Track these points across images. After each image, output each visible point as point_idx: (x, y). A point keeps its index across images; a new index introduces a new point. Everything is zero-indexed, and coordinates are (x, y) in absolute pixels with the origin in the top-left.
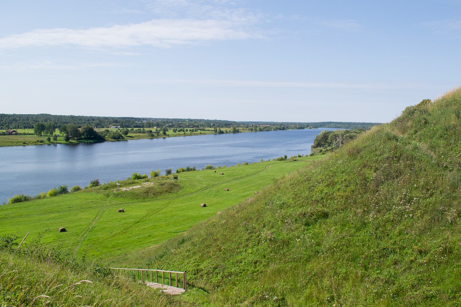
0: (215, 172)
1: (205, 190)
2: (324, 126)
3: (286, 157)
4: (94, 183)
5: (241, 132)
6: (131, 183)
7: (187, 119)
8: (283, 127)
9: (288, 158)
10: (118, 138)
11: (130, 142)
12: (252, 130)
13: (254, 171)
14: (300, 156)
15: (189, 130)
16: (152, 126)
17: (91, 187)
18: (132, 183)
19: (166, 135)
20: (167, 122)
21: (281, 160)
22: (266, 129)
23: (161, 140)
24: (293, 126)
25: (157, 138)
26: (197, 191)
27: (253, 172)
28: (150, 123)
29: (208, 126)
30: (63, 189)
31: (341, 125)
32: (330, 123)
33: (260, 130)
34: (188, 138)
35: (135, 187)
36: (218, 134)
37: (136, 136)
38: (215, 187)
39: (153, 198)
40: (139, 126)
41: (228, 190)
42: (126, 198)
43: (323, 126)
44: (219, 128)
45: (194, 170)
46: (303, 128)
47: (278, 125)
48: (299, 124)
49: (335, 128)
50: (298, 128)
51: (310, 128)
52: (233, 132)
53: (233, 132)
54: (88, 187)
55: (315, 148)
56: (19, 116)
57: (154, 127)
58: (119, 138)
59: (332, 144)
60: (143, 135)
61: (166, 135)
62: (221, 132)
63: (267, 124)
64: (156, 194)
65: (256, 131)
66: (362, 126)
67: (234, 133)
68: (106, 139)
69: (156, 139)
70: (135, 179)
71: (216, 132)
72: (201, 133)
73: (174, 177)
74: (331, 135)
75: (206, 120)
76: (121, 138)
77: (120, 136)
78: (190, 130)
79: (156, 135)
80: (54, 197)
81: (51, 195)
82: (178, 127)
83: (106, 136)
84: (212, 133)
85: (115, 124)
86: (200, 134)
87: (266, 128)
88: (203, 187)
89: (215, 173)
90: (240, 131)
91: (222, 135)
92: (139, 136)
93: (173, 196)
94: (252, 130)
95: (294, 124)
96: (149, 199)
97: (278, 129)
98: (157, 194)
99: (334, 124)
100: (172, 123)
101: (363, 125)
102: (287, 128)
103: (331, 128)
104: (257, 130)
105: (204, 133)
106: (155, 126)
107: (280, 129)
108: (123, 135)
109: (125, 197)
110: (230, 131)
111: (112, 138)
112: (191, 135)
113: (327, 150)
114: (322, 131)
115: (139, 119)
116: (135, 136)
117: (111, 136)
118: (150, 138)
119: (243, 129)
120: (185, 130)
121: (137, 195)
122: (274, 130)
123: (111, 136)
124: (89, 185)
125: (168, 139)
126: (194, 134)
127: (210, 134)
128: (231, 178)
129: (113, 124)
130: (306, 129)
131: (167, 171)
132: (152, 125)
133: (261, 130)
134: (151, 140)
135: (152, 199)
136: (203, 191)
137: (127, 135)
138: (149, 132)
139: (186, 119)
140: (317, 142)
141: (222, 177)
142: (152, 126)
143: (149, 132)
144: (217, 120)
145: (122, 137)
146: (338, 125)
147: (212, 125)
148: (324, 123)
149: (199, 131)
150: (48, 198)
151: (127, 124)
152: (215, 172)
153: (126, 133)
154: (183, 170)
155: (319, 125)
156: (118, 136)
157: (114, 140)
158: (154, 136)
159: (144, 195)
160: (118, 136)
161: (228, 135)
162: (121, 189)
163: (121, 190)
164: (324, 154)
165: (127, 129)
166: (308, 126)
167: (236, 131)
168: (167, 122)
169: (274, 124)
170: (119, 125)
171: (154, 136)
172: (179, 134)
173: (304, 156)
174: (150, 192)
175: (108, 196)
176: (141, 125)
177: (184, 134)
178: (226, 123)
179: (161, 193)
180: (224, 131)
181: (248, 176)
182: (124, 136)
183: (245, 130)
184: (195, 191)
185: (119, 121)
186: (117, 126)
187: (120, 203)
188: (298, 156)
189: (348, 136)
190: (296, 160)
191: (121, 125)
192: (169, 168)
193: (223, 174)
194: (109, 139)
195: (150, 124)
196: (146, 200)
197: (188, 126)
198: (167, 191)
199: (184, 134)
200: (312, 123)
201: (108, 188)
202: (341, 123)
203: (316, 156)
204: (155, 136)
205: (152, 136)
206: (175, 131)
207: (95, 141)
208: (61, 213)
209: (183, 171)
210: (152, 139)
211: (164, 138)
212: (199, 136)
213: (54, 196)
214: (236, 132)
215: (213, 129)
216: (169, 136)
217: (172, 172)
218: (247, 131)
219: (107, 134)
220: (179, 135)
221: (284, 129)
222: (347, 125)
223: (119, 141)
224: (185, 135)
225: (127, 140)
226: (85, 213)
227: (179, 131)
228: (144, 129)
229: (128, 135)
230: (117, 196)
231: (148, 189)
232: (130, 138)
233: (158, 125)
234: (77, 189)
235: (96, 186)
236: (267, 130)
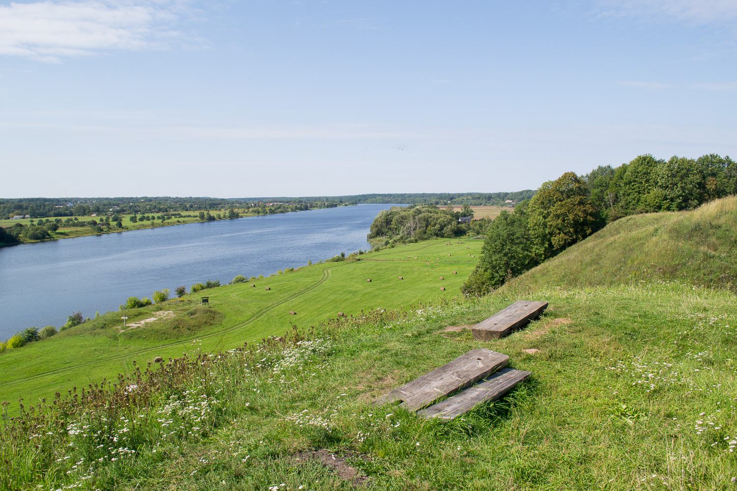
0: (254, 286)
1: (260, 316)
2: (366, 201)
3: (343, 255)
4: (73, 320)
5: (242, 217)
6: (137, 314)
7: (142, 198)
8: (304, 205)
9: (346, 257)
10: (41, 237)
11: (62, 242)
12: (259, 213)
13: (312, 280)
14: (361, 253)
15: (156, 218)
16: (89, 212)
17: (71, 326)
18: (139, 315)
19: (123, 228)
20: (110, 204)
21: (337, 261)
22: (280, 210)
23: (113, 236)
24: (319, 203)
25: (107, 233)
26: (250, 319)
27: (312, 282)
28: (84, 207)
29: (183, 209)
30: (32, 333)
31: (391, 198)
32: (374, 196)
33: (271, 213)
34: (158, 231)
35: (147, 320)
36: (206, 222)
37: (72, 232)
38: (272, 310)
39: (190, 335)
40: (63, 213)
41: (295, 314)
42: (147, 339)
43: (364, 201)
44: (207, 210)
45: (217, 285)
46: (336, 206)
47: (295, 202)
48: (327, 199)
49: (383, 203)
50: (328, 207)
51: (346, 205)
52: (230, 217)
53: (230, 217)
54: (66, 326)
55: (373, 237)
56: (32, 204)
57: (92, 214)
58: (44, 237)
59: (399, 231)
60: (84, 230)
61: (123, 228)
62: (211, 219)
63: (277, 202)
64: (192, 328)
65: (265, 213)
66: (422, 198)
67: (231, 219)
68: (22, 240)
69: (106, 235)
70: (134, 306)
71: (203, 219)
72: (179, 222)
73: (203, 300)
74: (396, 217)
75: (174, 199)
76: (47, 237)
77: (45, 235)
78: (159, 218)
79: (105, 228)
80: (22, 349)
81: (16, 346)
82: (134, 213)
83: (20, 234)
84: (197, 220)
85: (19, 211)
86: (178, 223)
87: (279, 208)
88: (255, 312)
89: (255, 288)
90: (240, 215)
91: (212, 223)
92: (77, 231)
93: (220, 330)
94: (259, 213)
95: (319, 199)
96: (185, 337)
97: (299, 209)
98: (194, 328)
99: (380, 198)
100: (118, 205)
101: (423, 197)
102: (312, 206)
103: (376, 203)
104: (267, 213)
105: (184, 222)
106: (93, 212)
107: (301, 209)
108: (49, 232)
109: (145, 338)
110: (224, 216)
111: (31, 238)
112: (163, 226)
113: (395, 241)
114: (379, 212)
115: (58, 201)
116: (70, 232)
117: (28, 234)
118: (96, 233)
119: (244, 212)
120: (151, 217)
121: (164, 333)
122: (292, 210)
123: (28, 234)
124: (67, 323)
125: (125, 234)
126: (168, 223)
127: (193, 222)
128: (286, 295)
129: (16, 212)
130: (315, 212)
131: (178, 291)
132: (88, 210)
133: (272, 212)
134: (99, 237)
135: (189, 338)
136: (257, 317)
137: (56, 232)
138: (91, 224)
139: (140, 198)
140: (375, 230)
141: (268, 294)
142: (89, 212)
143: (91, 224)
144: (193, 197)
145: (49, 235)
146: (387, 199)
147: (188, 206)
148: (364, 196)
149: (174, 219)
150: (11, 351)
151: (41, 211)
152: (254, 286)
153: (55, 228)
154: (201, 286)
155: (358, 199)
156: (41, 234)
157: (32, 241)
158: (102, 230)
159: (175, 331)
160: (41, 234)
161: (222, 222)
162: (130, 325)
163: (129, 327)
164: (393, 247)
165: (108, 216)
166: (341, 202)
167: (234, 216)
168: (110, 204)
169: (289, 201)
170: (27, 214)
171: (102, 230)
172: (143, 225)
173: (367, 252)
174: (181, 327)
175: (116, 338)
176: (67, 212)
177: (152, 225)
178: (210, 202)
179: (199, 327)
180: (215, 216)
181: (308, 289)
182: (51, 234)
183: (247, 213)
184: (246, 318)
185: (24, 207)
186: (25, 216)
187: (144, 348)
188: (359, 252)
189: (422, 218)
190: (359, 260)
191: (31, 213)
192: (181, 286)
193: (270, 289)
194: (26, 239)
195: (85, 210)
196: (181, 340)
197: (150, 209)
198: (206, 323)
199: (153, 224)
200: (346, 197)
201: (105, 325)
202: (391, 195)
203: (383, 251)
204: (104, 230)
205: (99, 230)
206: (133, 219)
207: (5, 244)
208: (59, 374)
209: (203, 288)
210: (99, 235)
211: (120, 233)
212: (176, 227)
213: (21, 346)
214: (234, 217)
215: (197, 213)
216: (127, 228)
217: (187, 291)
218: (251, 214)
219: (21, 230)
220: (145, 227)
221: (306, 208)
222: (400, 199)
223: (44, 242)
224: (153, 226)
225: (56, 240)
226: (101, 369)
227: (141, 219)
228: (76, 219)
229: (58, 231)
230: (131, 337)
231: (177, 323)
232: (63, 236)
233: (98, 211)
234: (51, 333)
235: (79, 323)
236: (282, 212)
